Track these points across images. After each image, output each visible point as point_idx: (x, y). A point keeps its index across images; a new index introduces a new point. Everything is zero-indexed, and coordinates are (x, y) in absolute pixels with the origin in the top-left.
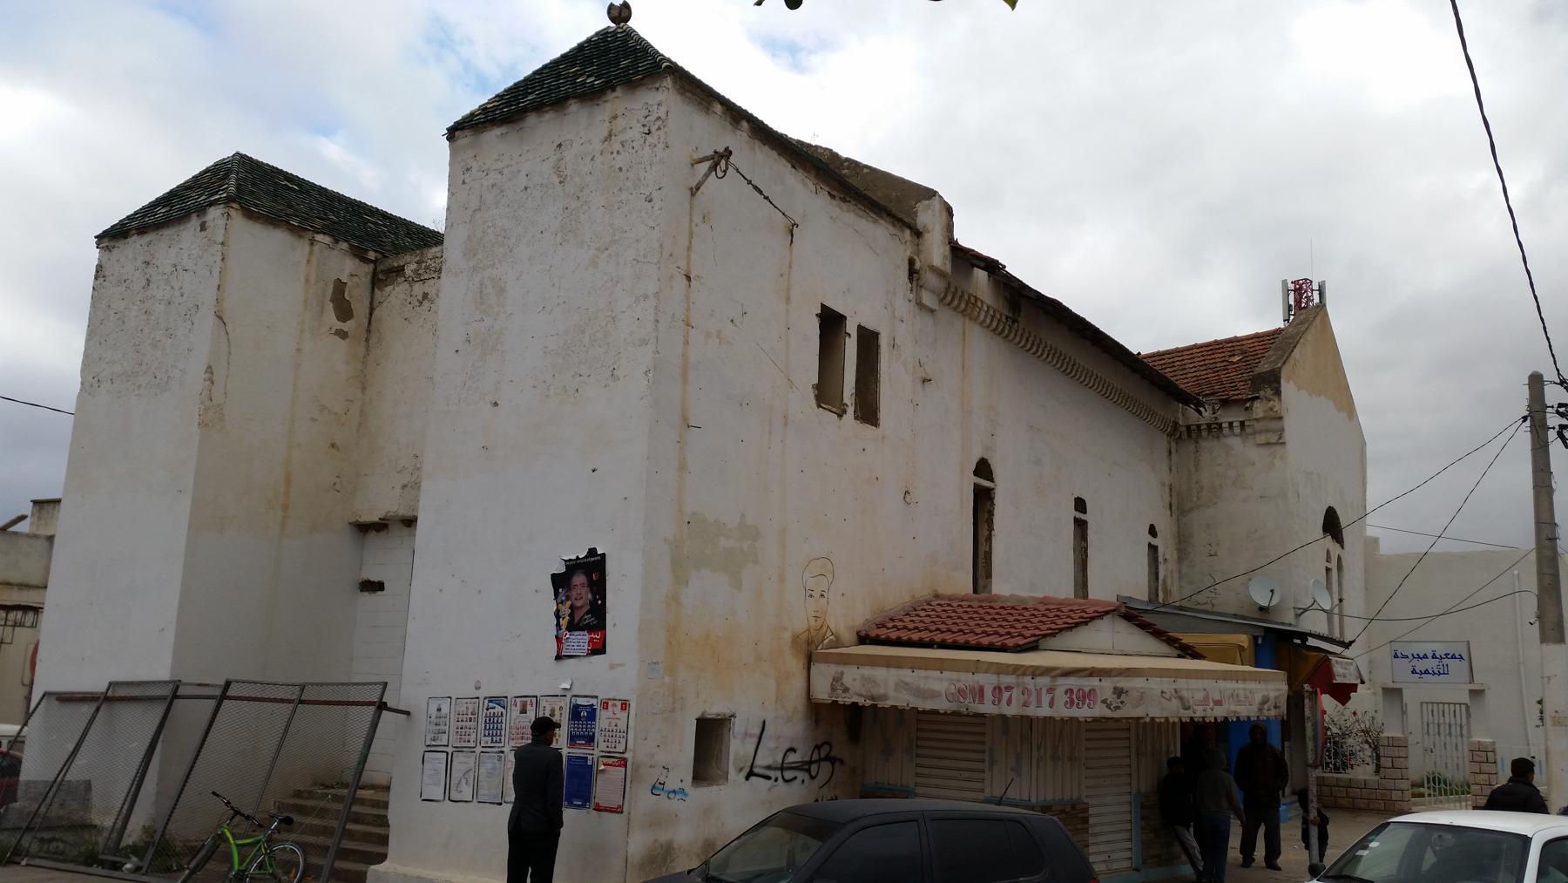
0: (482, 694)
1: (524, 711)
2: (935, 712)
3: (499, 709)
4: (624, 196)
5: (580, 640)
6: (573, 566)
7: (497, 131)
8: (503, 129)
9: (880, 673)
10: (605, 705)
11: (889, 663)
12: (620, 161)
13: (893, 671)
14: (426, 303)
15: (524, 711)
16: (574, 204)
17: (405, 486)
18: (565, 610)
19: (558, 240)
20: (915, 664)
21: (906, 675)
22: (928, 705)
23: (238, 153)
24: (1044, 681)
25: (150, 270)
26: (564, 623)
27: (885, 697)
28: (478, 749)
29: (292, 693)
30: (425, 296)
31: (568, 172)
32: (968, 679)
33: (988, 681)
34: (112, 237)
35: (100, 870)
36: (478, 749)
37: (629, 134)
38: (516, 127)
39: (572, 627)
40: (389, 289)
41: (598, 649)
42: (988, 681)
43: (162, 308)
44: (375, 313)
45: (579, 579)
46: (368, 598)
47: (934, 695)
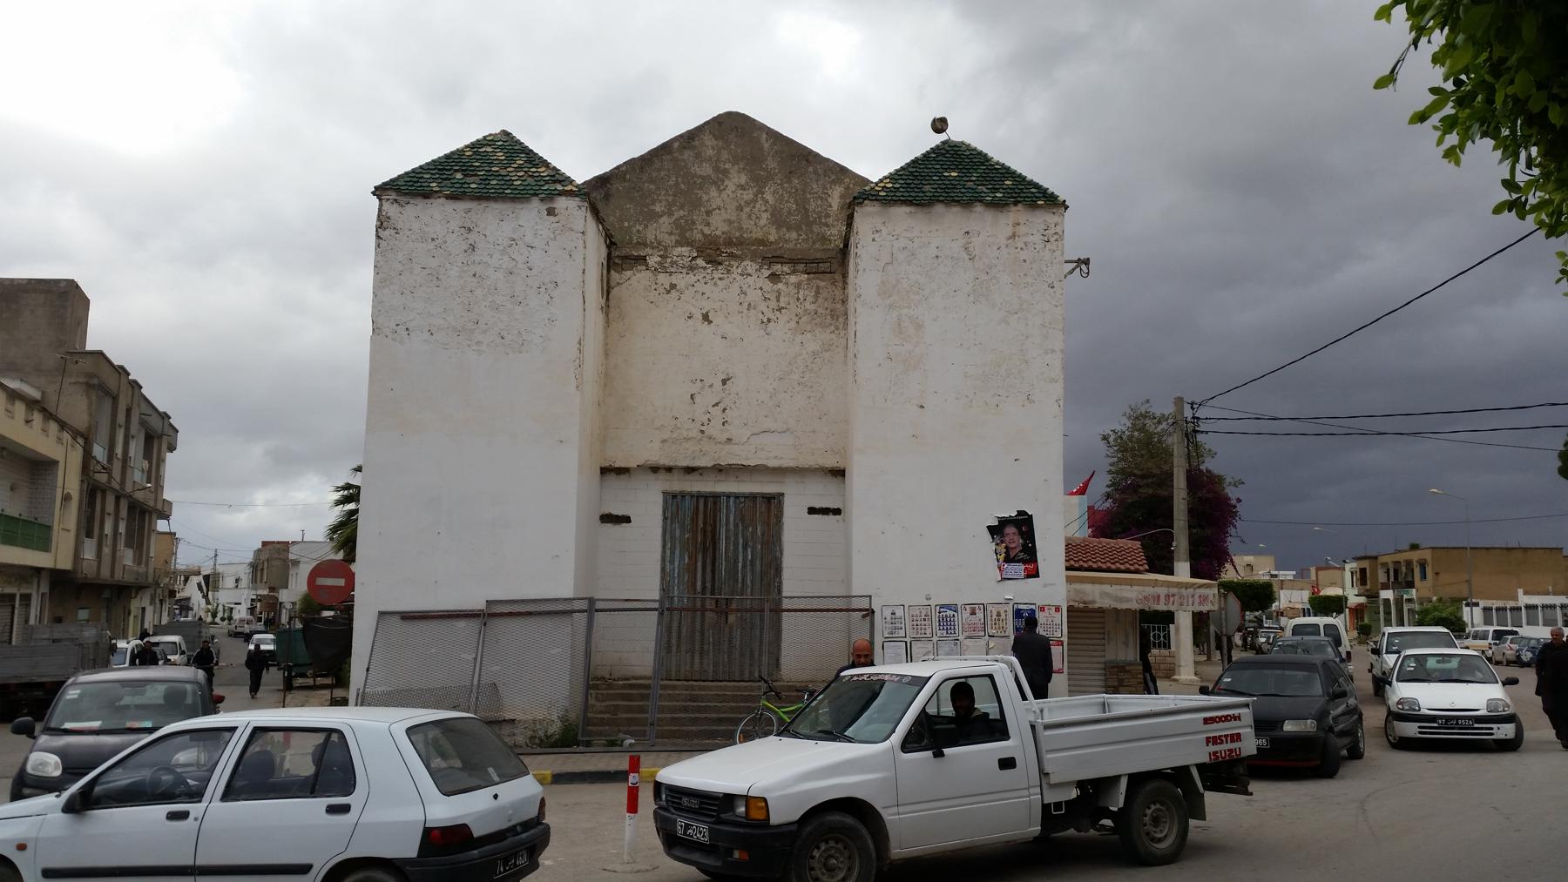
0: (933, 603)
1: (973, 613)
2: (1156, 612)
3: (950, 613)
4: (1029, 280)
5: (1020, 568)
6: (1004, 522)
7: (907, 209)
8: (912, 209)
9: (1088, 587)
10: (1042, 609)
11: (1093, 581)
12: (1024, 255)
13: (1097, 586)
14: (674, 293)
15: (973, 613)
16: (984, 277)
17: (664, 441)
18: (1002, 548)
19: (971, 299)
20: (1111, 582)
21: (1107, 588)
22: (1124, 606)
23: (506, 133)
24: (1190, 591)
25: (473, 237)
26: (1001, 558)
27: (1094, 602)
28: (935, 639)
29: (584, 605)
30: (673, 286)
31: (977, 252)
32: (1150, 590)
33: (1162, 591)
34: (405, 189)
35: (581, 749)
36: (935, 639)
37: (1030, 239)
38: (926, 210)
39: (1008, 560)
40: (629, 273)
41: (1034, 574)
42: (1162, 591)
43: (500, 275)
44: (614, 292)
45: (1010, 530)
46: (610, 528)
47: (1128, 600)
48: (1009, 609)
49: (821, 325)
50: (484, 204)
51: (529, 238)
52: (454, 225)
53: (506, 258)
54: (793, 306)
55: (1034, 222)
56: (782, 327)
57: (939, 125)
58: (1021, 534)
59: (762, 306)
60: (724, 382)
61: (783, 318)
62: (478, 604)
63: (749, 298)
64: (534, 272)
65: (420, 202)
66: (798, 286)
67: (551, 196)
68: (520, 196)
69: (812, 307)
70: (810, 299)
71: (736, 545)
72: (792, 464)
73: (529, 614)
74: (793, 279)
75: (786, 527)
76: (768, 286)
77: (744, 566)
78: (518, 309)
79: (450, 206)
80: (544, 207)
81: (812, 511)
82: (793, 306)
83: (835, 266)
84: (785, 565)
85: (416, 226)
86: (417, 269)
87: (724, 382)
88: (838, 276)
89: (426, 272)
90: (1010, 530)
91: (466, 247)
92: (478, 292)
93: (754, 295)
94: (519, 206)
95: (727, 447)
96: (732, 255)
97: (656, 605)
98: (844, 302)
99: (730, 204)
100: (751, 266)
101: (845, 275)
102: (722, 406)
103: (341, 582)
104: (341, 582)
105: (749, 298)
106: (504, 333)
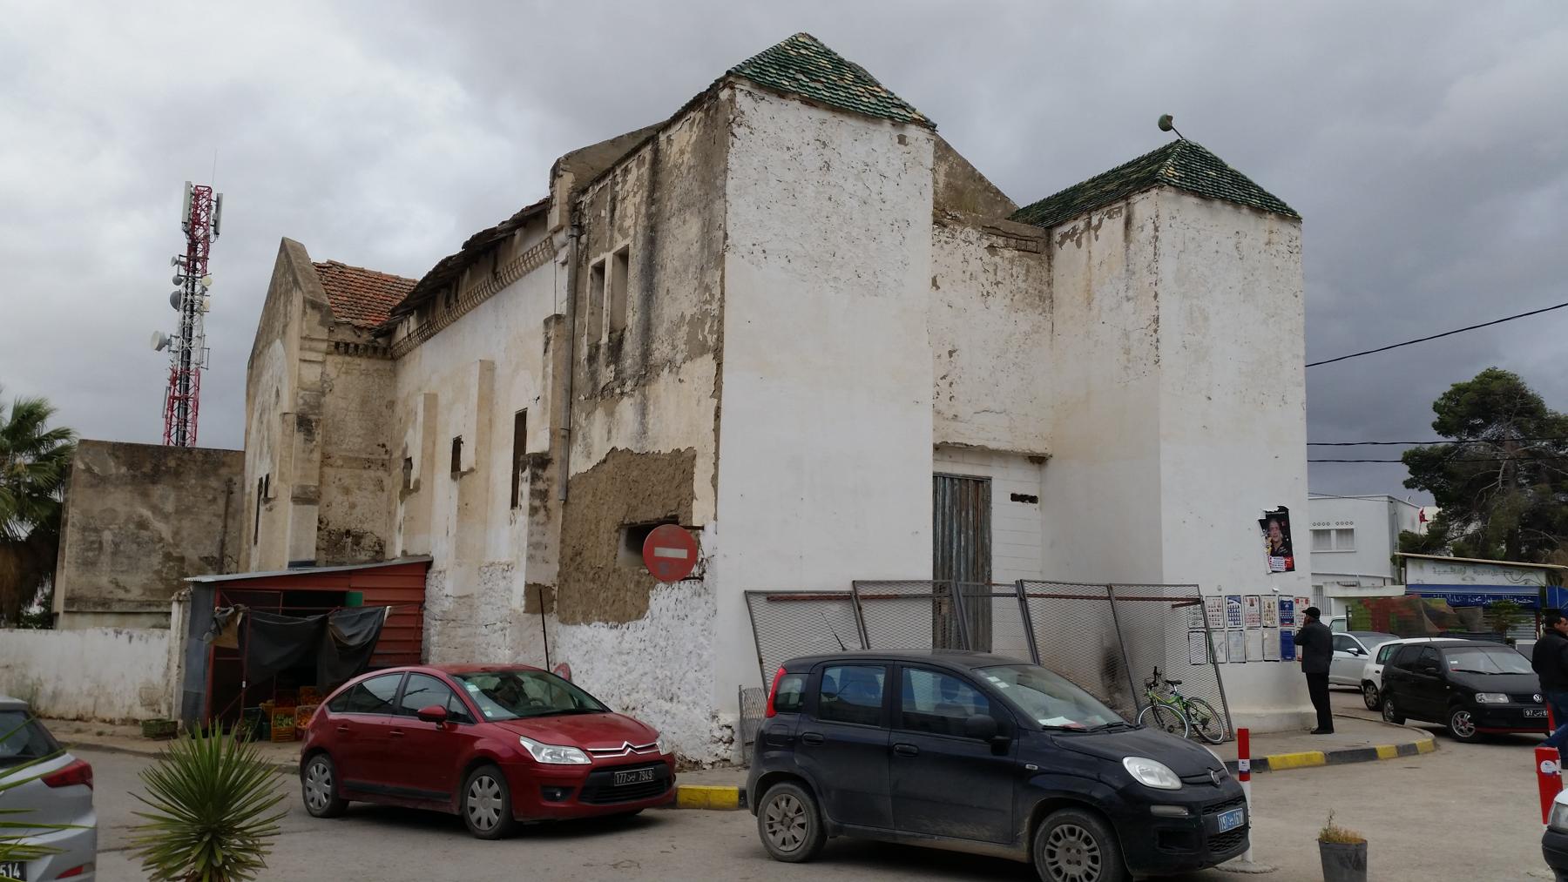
0: (1223, 594)
43: (855, 203)
45: (1274, 524)
48: (1276, 600)
49: (1031, 305)
50: (840, 117)
51: (882, 166)
52: (809, 136)
53: (860, 184)
54: (1007, 282)
55: (1285, 230)
56: (999, 301)
57: (1166, 124)
58: (1281, 528)
59: (982, 278)
60: (951, 353)
61: (1001, 292)
62: (846, 587)
63: (970, 268)
64: (888, 206)
65: (774, 99)
66: (1012, 261)
67: (906, 122)
68: (872, 117)
69: (1023, 286)
70: (1022, 277)
71: (951, 530)
72: (1008, 447)
73: (897, 597)
74: (1007, 253)
75: (994, 512)
76: (987, 256)
77: (958, 552)
78: (873, 245)
79: (807, 113)
80: (896, 133)
81: (1015, 497)
82: (1007, 282)
83: (1041, 247)
84: (994, 553)
85: (771, 129)
86: (773, 183)
87: (951, 353)
88: (1044, 257)
89: (783, 186)
90: (1274, 524)
91: (821, 164)
92: (834, 219)
93: (975, 266)
94: (872, 127)
95: (954, 424)
96: (955, 218)
97: (1013, 591)
98: (1050, 284)
99: (1169, 170)
100: (974, 235)
101: (1050, 257)
102: (949, 379)
103: (682, 554)
104: (682, 554)
105: (970, 268)
106: (860, 271)
